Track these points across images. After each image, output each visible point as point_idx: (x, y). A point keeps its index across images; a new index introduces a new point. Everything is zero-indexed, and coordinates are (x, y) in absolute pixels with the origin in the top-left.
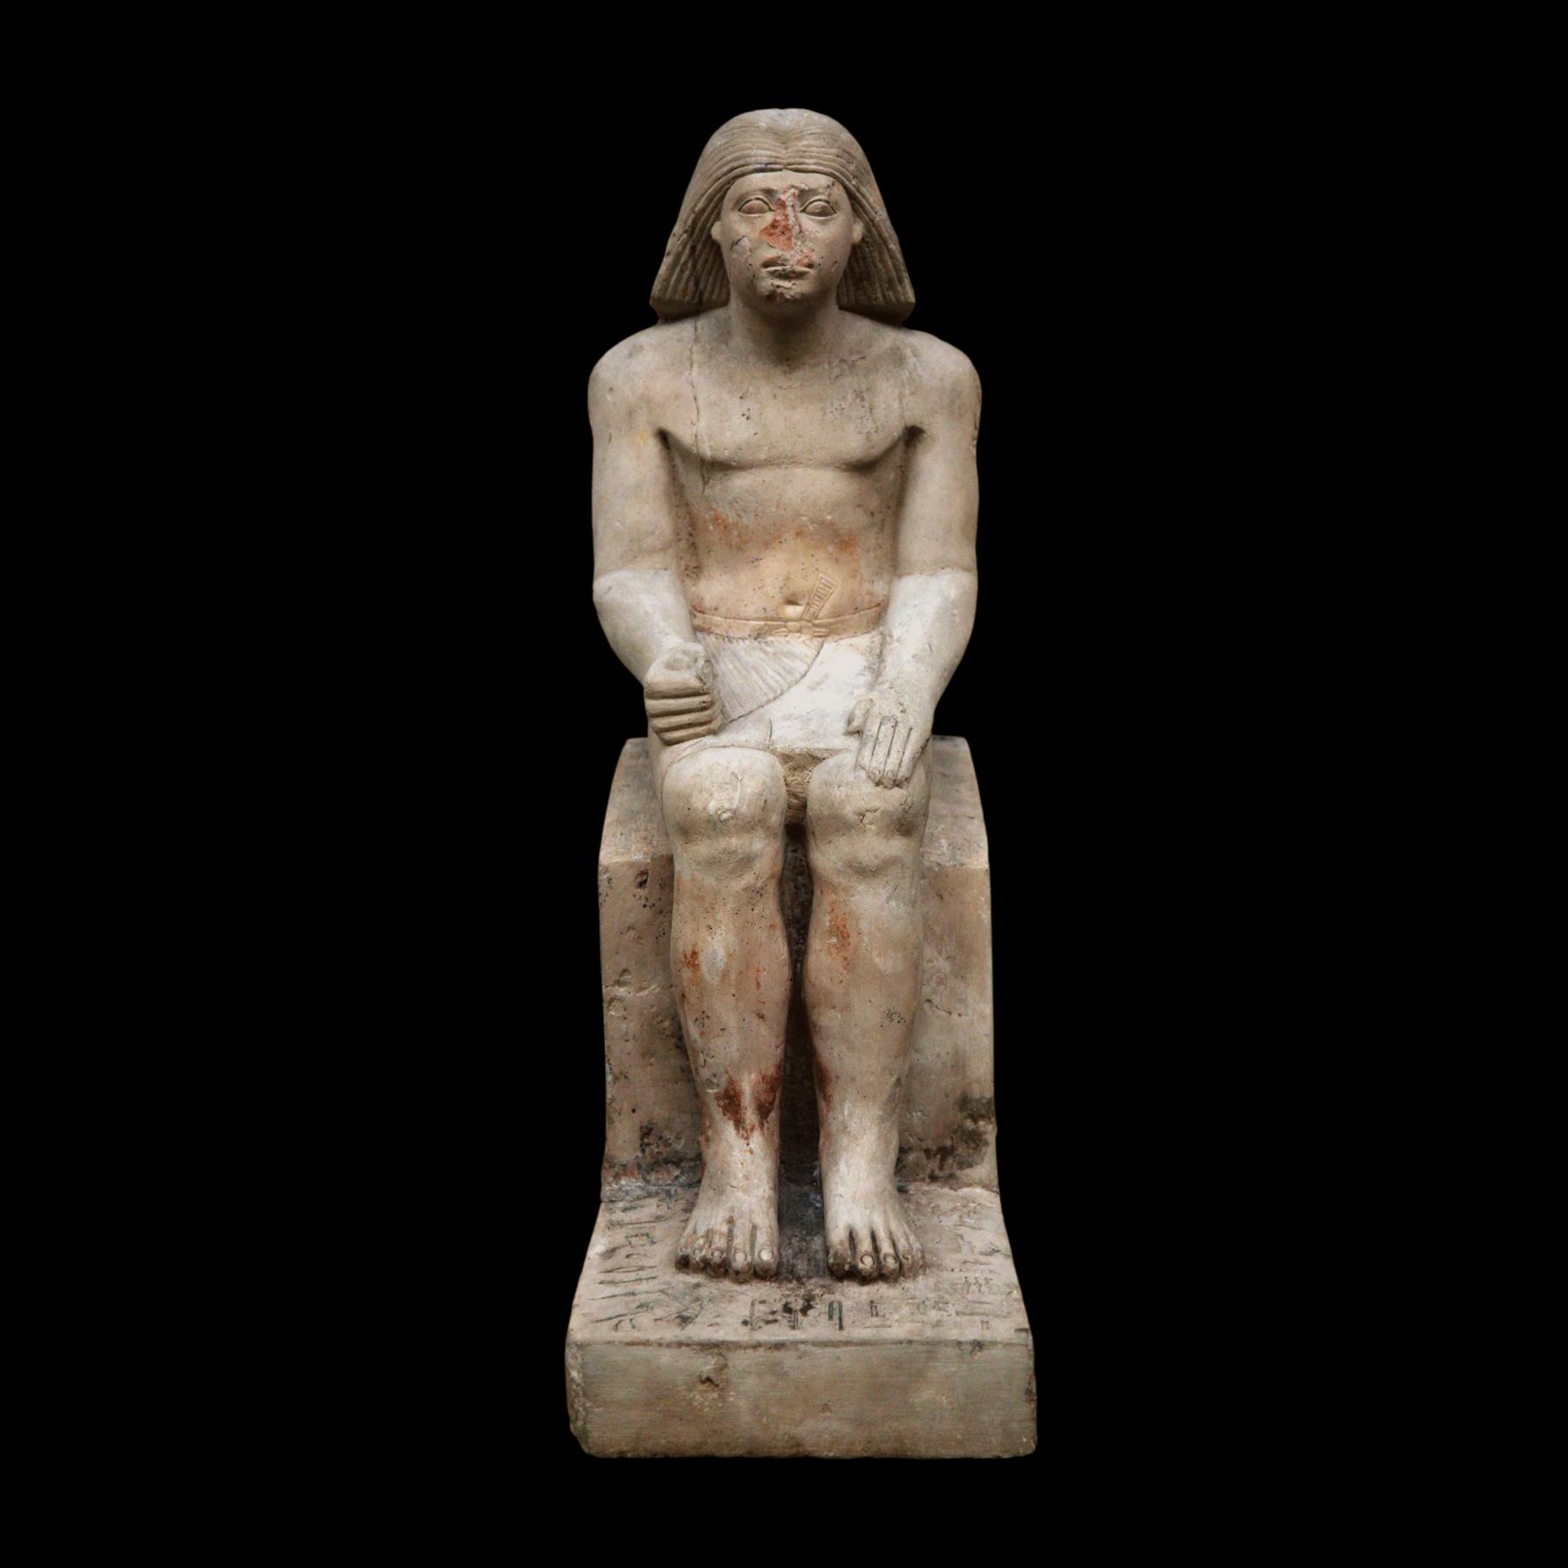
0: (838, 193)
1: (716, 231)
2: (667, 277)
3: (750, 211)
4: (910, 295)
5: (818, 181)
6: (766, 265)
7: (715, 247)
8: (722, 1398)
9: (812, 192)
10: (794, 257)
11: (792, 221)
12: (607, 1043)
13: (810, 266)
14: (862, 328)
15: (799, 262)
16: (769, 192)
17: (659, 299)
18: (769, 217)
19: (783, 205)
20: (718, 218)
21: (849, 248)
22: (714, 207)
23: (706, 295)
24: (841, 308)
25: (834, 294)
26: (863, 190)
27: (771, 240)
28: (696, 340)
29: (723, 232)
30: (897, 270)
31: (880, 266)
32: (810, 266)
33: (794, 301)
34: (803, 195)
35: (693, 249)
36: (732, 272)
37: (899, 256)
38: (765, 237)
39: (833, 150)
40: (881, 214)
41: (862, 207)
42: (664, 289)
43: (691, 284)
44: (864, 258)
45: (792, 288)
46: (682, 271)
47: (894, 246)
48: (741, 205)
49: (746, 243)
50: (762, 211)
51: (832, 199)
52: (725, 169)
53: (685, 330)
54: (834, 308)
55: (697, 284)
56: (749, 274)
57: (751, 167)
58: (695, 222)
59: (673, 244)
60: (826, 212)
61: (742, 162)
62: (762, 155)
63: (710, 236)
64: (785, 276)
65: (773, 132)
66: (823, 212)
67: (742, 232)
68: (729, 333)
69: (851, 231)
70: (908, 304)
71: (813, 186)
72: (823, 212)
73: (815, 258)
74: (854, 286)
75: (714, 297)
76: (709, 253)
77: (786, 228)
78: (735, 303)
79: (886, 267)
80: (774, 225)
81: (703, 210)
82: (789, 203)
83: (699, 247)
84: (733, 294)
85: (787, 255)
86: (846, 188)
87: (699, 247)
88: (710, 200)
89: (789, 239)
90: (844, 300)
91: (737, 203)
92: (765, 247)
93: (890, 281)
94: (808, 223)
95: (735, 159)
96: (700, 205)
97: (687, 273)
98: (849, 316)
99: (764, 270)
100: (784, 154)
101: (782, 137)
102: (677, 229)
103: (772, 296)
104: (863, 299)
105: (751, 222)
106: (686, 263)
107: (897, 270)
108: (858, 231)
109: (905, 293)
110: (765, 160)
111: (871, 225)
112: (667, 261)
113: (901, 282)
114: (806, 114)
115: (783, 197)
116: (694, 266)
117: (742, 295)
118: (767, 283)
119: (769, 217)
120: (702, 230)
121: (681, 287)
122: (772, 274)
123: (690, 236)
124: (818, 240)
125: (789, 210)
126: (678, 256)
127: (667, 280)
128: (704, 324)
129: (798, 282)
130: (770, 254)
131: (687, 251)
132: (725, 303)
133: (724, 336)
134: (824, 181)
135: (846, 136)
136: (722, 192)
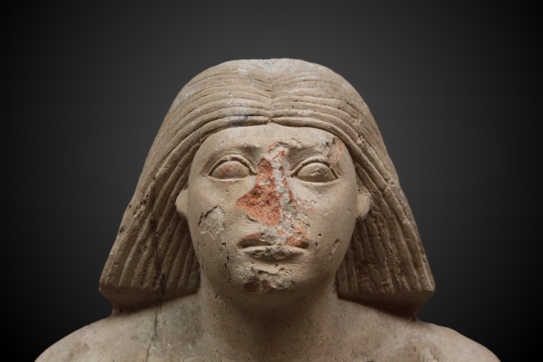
0: (340, 153)
1: (182, 202)
2: (120, 256)
3: (224, 175)
4: (430, 284)
5: (314, 138)
6: (244, 244)
7: (181, 222)
8: (245, 268)
9: (306, 150)
10: (283, 234)
11: (279, 187)
12: (183, 89)
13: (304, 245)
14: (369, 320)
15: (288, 240)
16: (249, 150)
17: (109, 287)
18: (249, 182)
19: (267, 166)
20: (184, 184)
21: (354, 222)
22: (179, 173)
23: (171, 279)
24: (341, 297)
25: (333, 280)
26: (371, 151)
27: (250, 212)
28: (155, 338)
30: (413, 251)
31: (391, 246)
32: (304, 245)
33: (282, 291)
34: (295, 154)
35: (153, 224)
36: (201, 253)
37: (415, 233)
38: (243, 208)
39: (333, 101)
40: (392, 181)
41: (370, 172)
42: (116, 274)
43: (151, 268)
44: (371, 236)
45: (279, 275)
46: (139, 251)
47: (409, 222)
48: (213, 167)
49: (218, 215)
50: (239, 175)
51: (333, 160)
52: (193, 124)
53: (141, 324)
54: (332, 296)
55: (158, 267)
56: (222, 256)
57: (226, 120)
58: (155, 190)
59: (129, 219)
60: (324, 176)
61: (215, 114)
62: (240, 103)
63: (174, 208)
64: (270, 258)
65: (258, 79)
66: (321, 177)
67: (214, 203)
68: (198, 330)
69: (355, 201)
70: (426, 292)
71: (307, 143)
72: (321, 177)
73: (310, 235)
74: (361, 270)
75: (181, 283)
76: (172, 228)
77: (272, 197)
78: (206, 292)
79: (398, 247)
80: (255, 193)
81: (165, 176)
82: (276, 165)
83: (161, 221)
84: (204, 281)
85: (273, 231)
86: (349, 148)
87: (161, 221)
88: (175, 162)
89: (276, 210)
90: (345, 286)
91: (208, 165)
92: (244, 221)
93: (403, 265)
94: (301, 189)
95: (207, 111)
96: (162, 170)
97: (145, 253)
98: (350, 307)
99: (242, 251)
100: (268, 104)
101: (270, 86)
102: (135, 200)
103: (252, 285)
104: (368, 286)
105: (224, 188)
106: (144, 241)
107: (413, 251)
108: (364, 202)
109: (422, 279)
110: (245, 110)
111: (380, 196)
112: (121, 238)
113: (417, 265)
114: (298, 63)
115: (268, 157)
116: (155, 245)
117: (213, 282)
118: (246, 268)
119: (249, 182)
120: (167, 195)
121: (138, 270)
122: (253, 255)
123: (150, 208)
124: (314, 212)
125: (276, 174)
126: (135, 232)
127: (120, 262)
128: (168, 316)
129: (287, 266)
130: (249, 229)
131: (145, 227)
132: (195, 291)
133: (191, 334)
134: (321, 137)
135: (347, 87)
136: (190, 151)
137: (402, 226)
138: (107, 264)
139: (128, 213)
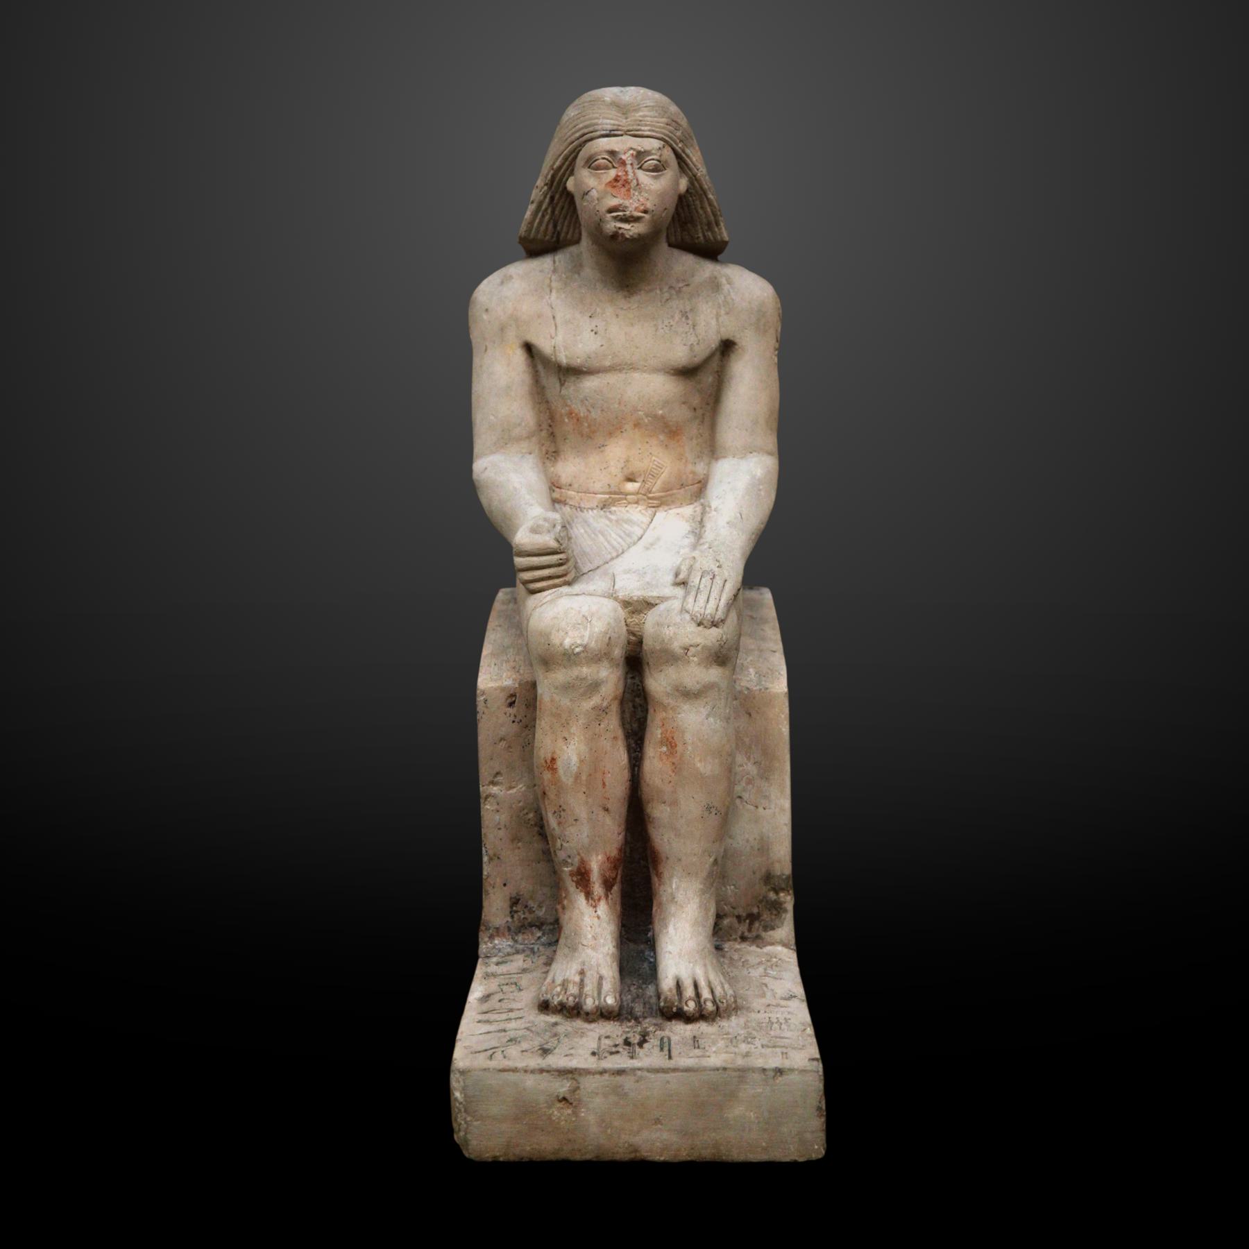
0: (668, 154)
1: (570, 184)
3: (598, 168)
5: (652, 144)
6: (610, 211)
7: (570, 197)
9: (647, 153)
10: (633, 205)
11: (630, 176)
13: (645, 212)
15: (636, 209)
16: (612, 153)
18: (612, 173)
19: (623, 163)
20: (572, 173)
21: (676, 198)
22: (568, 165)
23: (563, 235)
24: (670, 245)
25: (664, 235)
26: (688, 151)
27: (614, 191)
28: (554, 271)
29: (576, 185)
31: (701, 212)
32: (645, 212)
33: (633, 240)
34: (640, 155)
35: (552, 198)
36: (583, 217)
38: (609, 189)
39: (664, 120)
41: (687, 165)
43: (551, 226)
44: (688, 206)
45: (631, 230)
46: (543, 216)
48: (590, 163)
49: (594, 193)
50: (607, 168)
51: (663, 159)
52: (577, 135)
54: (664, 245)
55: (555, 226)
56: (597, 219)
57: (598, 133)
58: (553, 177)
60: (658, 169)
61: (591, 129)
63: (565, 188)
64: (625, 220)
66: (655, 169)
67: (591, 185)
68: (581, 265)
69: (678, 184)
71: (647, 148)
72: (655, 169)
73: (649, 205)
75: (569, 236)
76: (563, 202)
77: (626, 181)
78: (585, 242)
79: (705, 212)
80: (616, 179)
81: (560, 168)
82: (629, 162)
83: (557, 196)
84: (584, 234)
85: (627, 203)
86: (674, 150)
87: (557, 196)
88: (566, 159)
89: (629, 190)
90: (673, 239)
91: (587, 161)
92: (609, 197)
93: (709, 224)
94: (644, 177)
95: (586, 127)
96: (558, 164)
97: (547, 217)
98: (676, 252)
99: (609, 215)
100: (624, 123)
101: (623, 109)
103: (615, 236)
104: (687, 238)
105: (598, 177)
106: (546, 210)
108: (683, 184)
109: (721, 234)
110: (609, 127)
111: (694, 180)
113: (717, 224)
114: (642, 90)
115: (624, 157)
116: (553, 212)
117: (591, 235)
118: (611, 226)
119: (612, 173)
120: (559, 183)
121: (543, 228)
122: (615, 218)
123: (550, 188)
125: (629, 168)
126: (540, 204)
127: (531, 223)
128: (561, 258)
129: (636, 225)
130: (614, 202)
131: (547, 200)
132: (578, 241)
133: (577, 267)
134: (656, 144)
135: (674, 108)
136: (575, 153)
137: (708, 199)
138: (615, 90)
139: (535, 192)
